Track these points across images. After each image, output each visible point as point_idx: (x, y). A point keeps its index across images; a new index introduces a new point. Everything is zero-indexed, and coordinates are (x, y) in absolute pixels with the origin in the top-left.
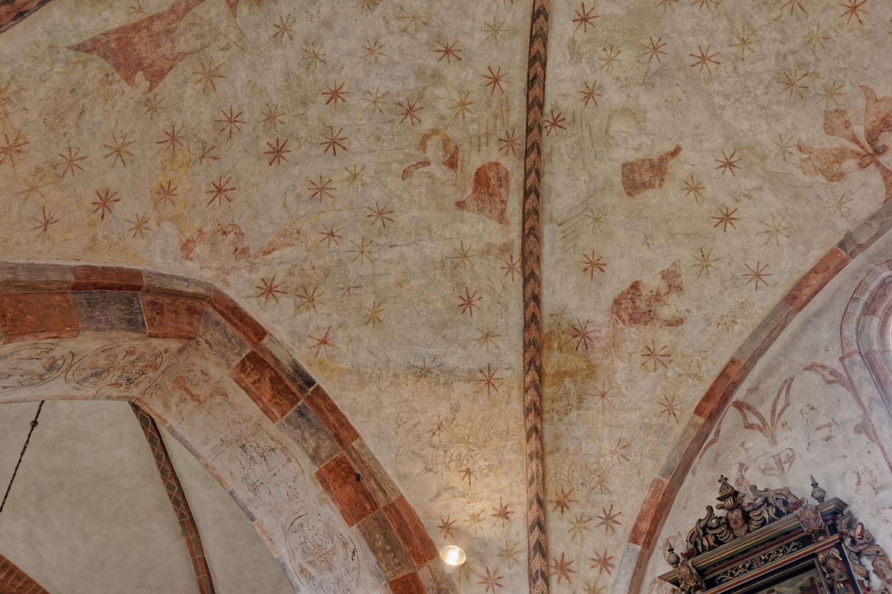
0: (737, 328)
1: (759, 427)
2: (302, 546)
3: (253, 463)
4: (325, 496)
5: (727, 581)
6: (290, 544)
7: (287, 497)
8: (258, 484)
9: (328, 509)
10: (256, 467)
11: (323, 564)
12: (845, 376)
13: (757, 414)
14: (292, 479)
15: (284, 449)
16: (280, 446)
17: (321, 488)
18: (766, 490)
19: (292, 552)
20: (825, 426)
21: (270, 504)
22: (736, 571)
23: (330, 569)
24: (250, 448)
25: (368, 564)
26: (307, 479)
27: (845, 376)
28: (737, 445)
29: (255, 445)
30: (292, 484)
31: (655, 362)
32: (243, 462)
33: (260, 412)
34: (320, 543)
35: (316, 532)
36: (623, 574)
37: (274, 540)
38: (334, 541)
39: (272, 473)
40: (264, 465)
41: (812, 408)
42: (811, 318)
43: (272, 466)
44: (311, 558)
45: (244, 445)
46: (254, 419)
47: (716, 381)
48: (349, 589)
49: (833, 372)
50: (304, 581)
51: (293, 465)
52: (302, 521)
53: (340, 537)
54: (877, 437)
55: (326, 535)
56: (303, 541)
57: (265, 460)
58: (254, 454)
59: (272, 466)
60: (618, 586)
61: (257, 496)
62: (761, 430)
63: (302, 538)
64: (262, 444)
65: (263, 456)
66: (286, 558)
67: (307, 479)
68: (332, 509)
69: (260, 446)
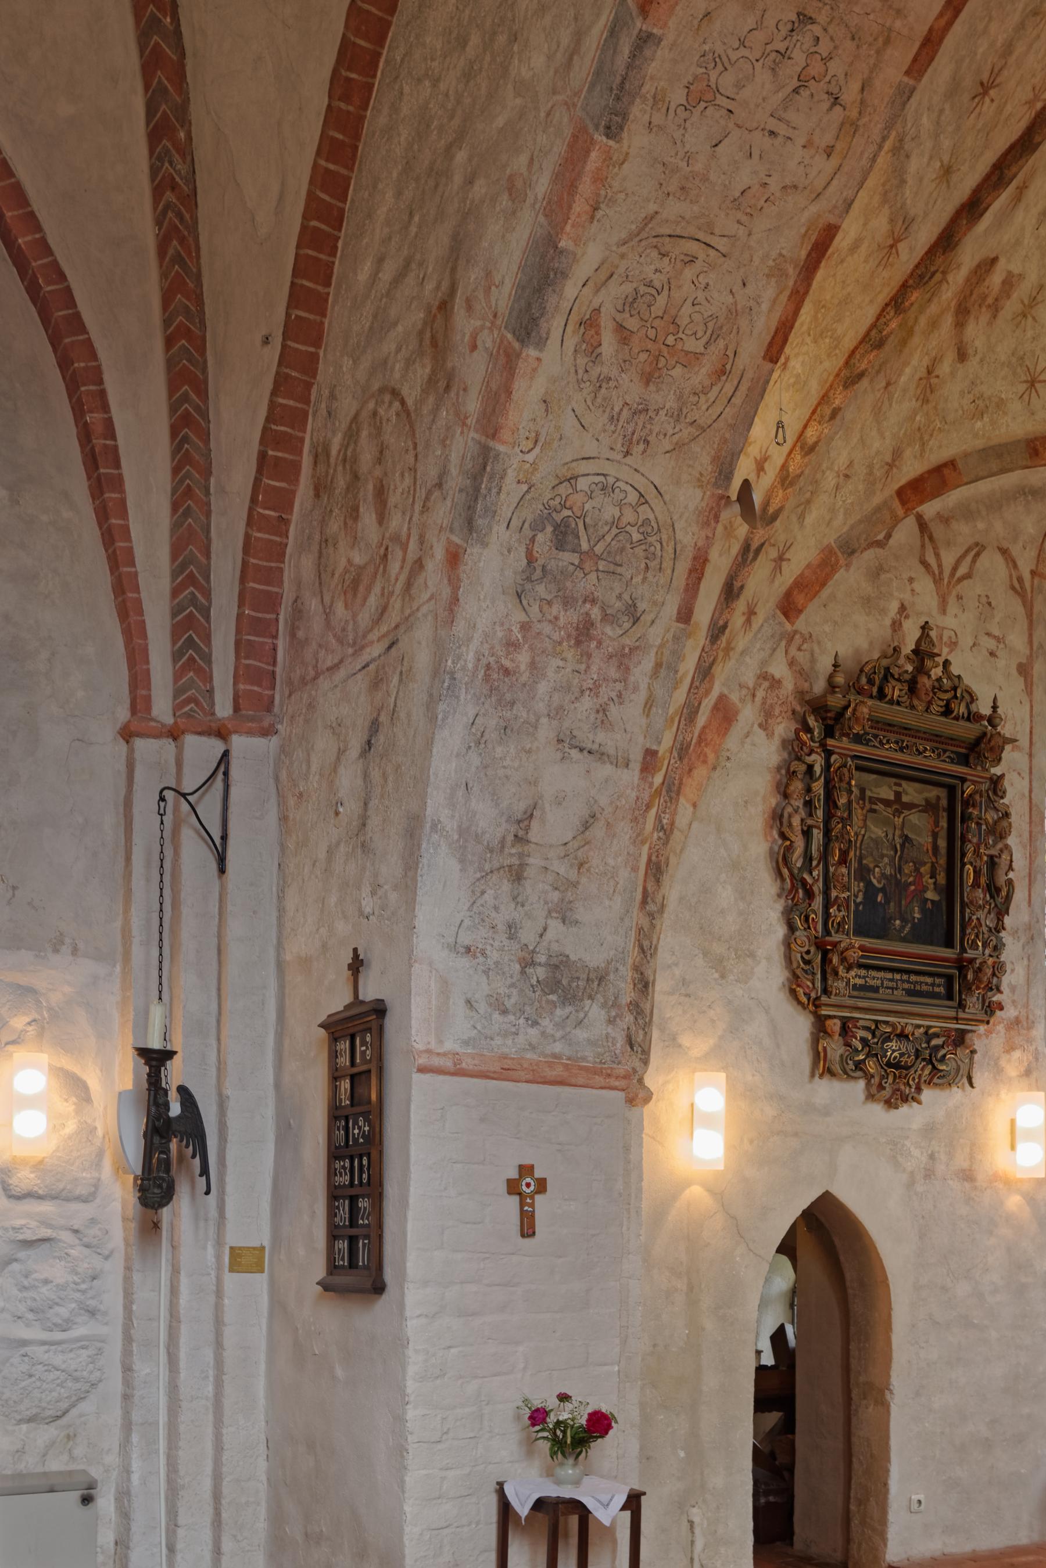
0: (979, 424)
1: (934, 574)
2: (643, 289)
3: (769, 61)
4: (792, 271)
5: (874, 746)
6: (623, 256)
7: (737, 194)
8: (721, 100)
9: (769, 293)
10: (763, 76)
11: (643, 356)
12: (1029, 595)
13: (937, 555)
14: (788, 181)
15: (850, 127)
16: (854, 114)
17: (804, 254)
18: (959, 677)
19: (606, 276)
20: (995, 637)
21: (688, 158)
22: (888, 742)
23: (647, 379)
24: (808, 41)
25: (726, 441)
26: (806, 214)
27: (1029, 595)
28: (905, 576)
29: (824, 48)
30: (774, 186)
31: (925, 386)
32: (760, 36)
33: (922, 30)
34: (683, 321)
35: (701, 298)
36: (758, 646)
37: (599, 214)
38: (712, 348)
39: (772, 124)
40: (781, 95)
41: (990, 604)
42: (1027, 490)
43: (791, 115)
44: (632, 324)
45: (812, 20)
46: (898, 24)
47: (930, 472)
48: (647, 442)
49: (1020, 580)
50: (571, 343)
51: (824, 166)
52: (702, 256)
53: (731, 354)
54: (1031, 693)
55: (711, 325)
56: (657, 284)
57: (796, 91)
58: (799, 57)
59: (791, 115)
60: (747, 659)
61: (687, 114)
62: (935, 582)
63: (664, 278)
64: (836, 67)
65: (803, 81)
66: (585, 267)
67: (806, 214)
68: (774, 302)
69: (831, 64)
